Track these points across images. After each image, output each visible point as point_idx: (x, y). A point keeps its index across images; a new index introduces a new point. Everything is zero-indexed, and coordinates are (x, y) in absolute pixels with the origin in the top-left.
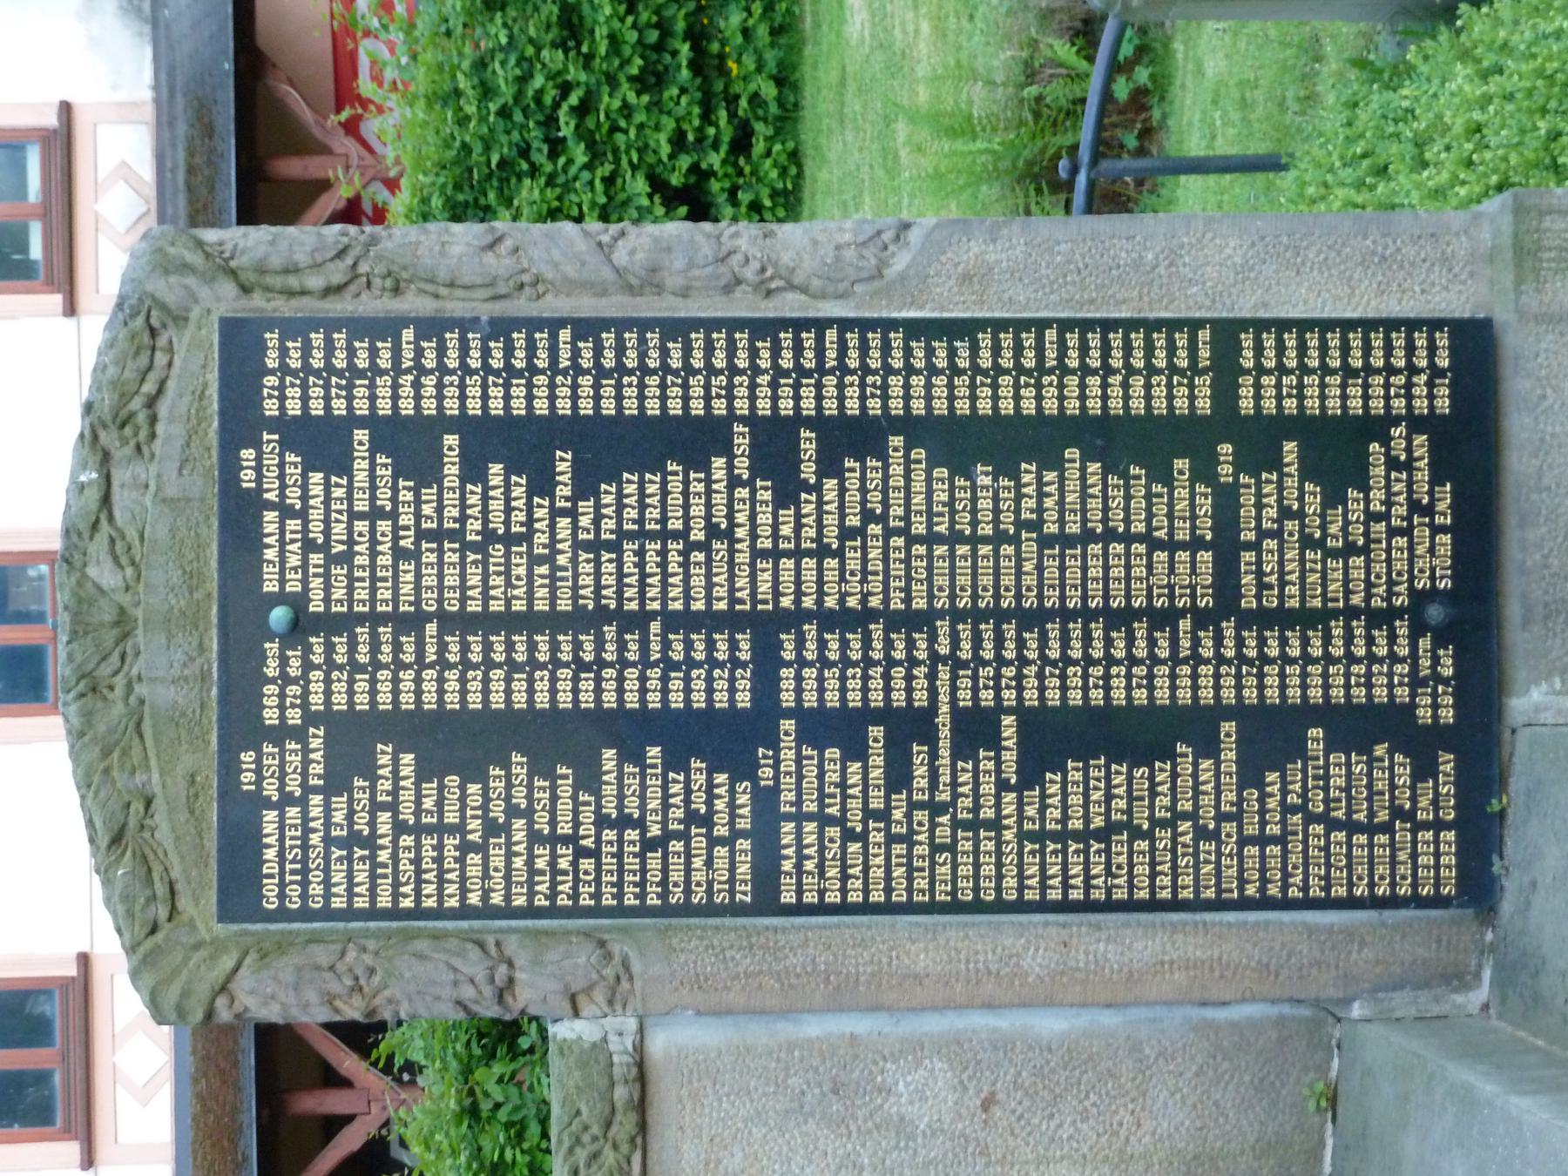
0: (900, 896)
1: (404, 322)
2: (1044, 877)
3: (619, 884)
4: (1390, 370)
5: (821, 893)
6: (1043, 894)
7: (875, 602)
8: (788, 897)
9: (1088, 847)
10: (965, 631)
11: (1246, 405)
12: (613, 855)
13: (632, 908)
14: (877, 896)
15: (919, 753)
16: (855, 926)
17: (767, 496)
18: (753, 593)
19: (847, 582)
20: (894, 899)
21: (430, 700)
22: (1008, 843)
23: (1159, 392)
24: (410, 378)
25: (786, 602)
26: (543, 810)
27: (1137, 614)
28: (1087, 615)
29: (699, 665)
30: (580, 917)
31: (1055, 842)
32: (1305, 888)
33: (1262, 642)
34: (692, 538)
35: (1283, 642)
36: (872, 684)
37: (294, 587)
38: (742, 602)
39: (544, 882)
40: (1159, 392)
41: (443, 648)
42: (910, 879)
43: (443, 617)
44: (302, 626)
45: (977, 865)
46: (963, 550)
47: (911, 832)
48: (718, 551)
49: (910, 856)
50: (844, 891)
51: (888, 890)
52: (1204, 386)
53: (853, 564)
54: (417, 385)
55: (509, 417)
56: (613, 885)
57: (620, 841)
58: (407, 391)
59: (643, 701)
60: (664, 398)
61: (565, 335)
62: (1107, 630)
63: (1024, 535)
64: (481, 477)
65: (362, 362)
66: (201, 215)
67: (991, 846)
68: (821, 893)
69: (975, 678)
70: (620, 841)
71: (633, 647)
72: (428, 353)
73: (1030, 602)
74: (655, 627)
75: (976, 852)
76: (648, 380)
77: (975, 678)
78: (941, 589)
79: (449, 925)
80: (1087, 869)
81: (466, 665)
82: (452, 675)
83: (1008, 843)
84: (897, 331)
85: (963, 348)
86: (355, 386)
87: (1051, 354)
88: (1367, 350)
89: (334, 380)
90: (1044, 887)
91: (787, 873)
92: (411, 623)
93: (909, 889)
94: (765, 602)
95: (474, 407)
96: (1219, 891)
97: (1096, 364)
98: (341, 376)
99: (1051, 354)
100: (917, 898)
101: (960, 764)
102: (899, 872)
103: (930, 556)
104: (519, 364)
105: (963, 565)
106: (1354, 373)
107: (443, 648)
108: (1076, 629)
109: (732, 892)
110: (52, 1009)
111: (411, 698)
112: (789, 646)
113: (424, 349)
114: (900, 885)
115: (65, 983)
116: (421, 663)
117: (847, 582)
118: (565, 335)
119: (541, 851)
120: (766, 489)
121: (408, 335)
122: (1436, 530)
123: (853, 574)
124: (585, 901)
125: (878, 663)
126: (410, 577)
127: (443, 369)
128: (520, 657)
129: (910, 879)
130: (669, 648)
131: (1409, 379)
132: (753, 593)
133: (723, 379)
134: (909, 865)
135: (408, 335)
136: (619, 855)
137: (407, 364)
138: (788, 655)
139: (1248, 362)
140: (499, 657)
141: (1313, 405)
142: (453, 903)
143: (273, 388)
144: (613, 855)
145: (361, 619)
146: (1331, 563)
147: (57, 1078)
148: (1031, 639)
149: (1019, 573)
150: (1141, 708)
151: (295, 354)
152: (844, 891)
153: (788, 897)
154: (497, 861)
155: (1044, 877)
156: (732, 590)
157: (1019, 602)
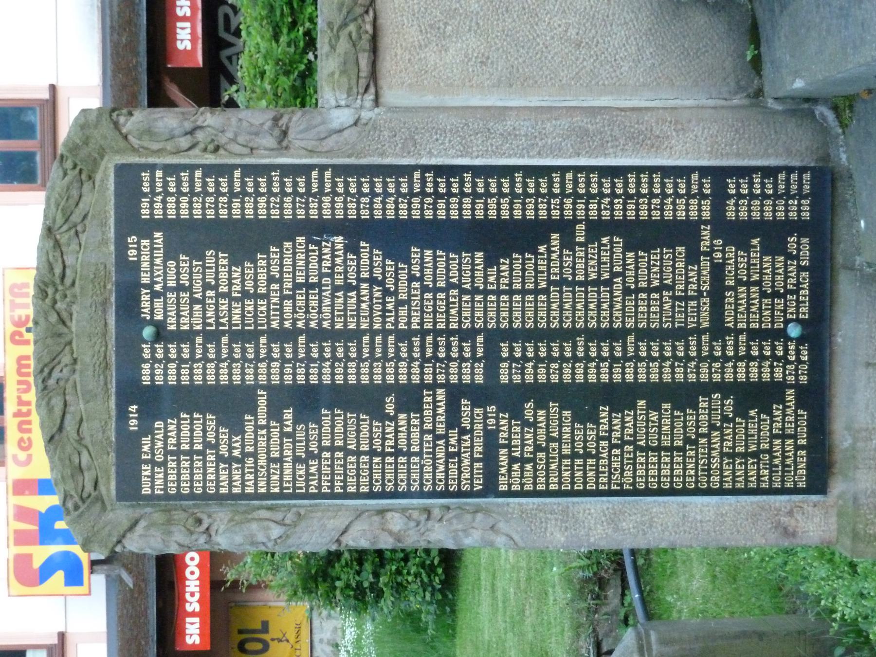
0: (591, 486)
1: (235, 167)
2: (231, 481)
3: (332, 481)
4: (652, 195)
5: (510, 485)
6: (243, 489)
7: (300, 324)
8: (503, 488)
9: (747, 461)
10: (442, 341)
11: (731, 215)
12: (328, 465)
13: (314, 494)
14: (565, 487)
15: (553, 407)
16: (608, 502)
17: (225, 262)
18: (230, 321)
19: (297, 313)
20: (576, 488)
21: (288, 379)
22: (714, 457)
23: (391, 206)
24: (160, 197)
25: (326, 325)
26: (378, 438)
27: (579, 332)
28: (449, 333)
29: (237, 361)
30: (537, 497)
31: (753, 458)
32: (319, 487)
33: (649, 348)
34: (220, 290)
35: (599, 349)
36: (413, 371)
37: (159, 317)
38: (211, 325)
39: (314, 480)
40: (391, 206)
41: (231, 351)
42: (597, 478)
43: (308, 331)
44: (161, 334)
45: (179, 475)
46: (479, 297)
47: (598, 452)
48: (170, 298)
49: (597, 465)
50: (535, 484)
51: (585, 483)
52: (706, 205)
53: (301, 303)
54: (164, 202)
55: (410, 220)
56: (328, 481)
57: (333, 458)
58: (158, 205)
59: (358, 379)
60: (191, 208)
61: (198, 173)
62: (586, 341)
63: (552, 289)
64: (356, 251)
65: (442, 190)
66: (132, 103)
67: (200, 464)
68: (510, 485)
69: (548, 368)
70: (333, 458)
71: (353, 350)
72: (454, 185)
73: (467, 325)
74: (199, 339)
75: (192, 467)
76: (286, 199)
77: (548, 368)
78: (567, 318)
79: (415, 502)
80: (746, 472)
81: (334, 359)
82: (403, 364)
83: (714, 457)
84: (556, 173)
85: (543, 183)
86: (590, 203)
87: (569, 186)
88: (638, 183)
89: (298, 199)
90: (230, 486)
91: (502, 475)
92: (212, 337)
93: (597, 483)
94: (237, 325)
95: (172, 214)
96: (282, 488)
97: (557, 191)
98: (302, 197)
99: (569, 186)
100: (601, 487)
101: (614, 415)
102: (590, 474)
103: (498, 302)
104: (632, 191)
105: (492, 306)
106: (631, 197)
107: (231, 351)
108: (442, 341)
109: (472, 484)
110: (35, 118)
111: (226, 377)
112: (505, 350)
113: (666, 183)
114: (301, 484)
115: (42, 103)
116: (360, 359)
117: (297, 313)
118: (198, 173)
119: (313, 463)
120: (224, 258)
121: (237, 173)
122: (150, 286)
123: (300, 308)
124: (325, 490)
125: (328, 360)
126: (238, 311)
127: (180, 193)
128: (543, 354)
129: (597, 478)
130: (463, 350)
131: (371, 200)
132: (230, 321)
133: (758, 202)
134: (597, 470)
135: (237, 173)
136: (332, 466)
137: (159, 190)
138: (505, 354)
139: (146, 189)
140: (173, 356)
141: (619, 215)
142: (263, 490)
143: (429, 204)
144: (328, 465)
145: (415, 333)
146: (234, 305)
147: (38, 158)
148: (404, 347)
149: (549, 310)
150: (365, 385)
151: (455, 185)
152: (535, 484)
153: (503, 488)
154: (541, 465)
155: (231, 481)
156: (204, 317)
157: (548, 325)
